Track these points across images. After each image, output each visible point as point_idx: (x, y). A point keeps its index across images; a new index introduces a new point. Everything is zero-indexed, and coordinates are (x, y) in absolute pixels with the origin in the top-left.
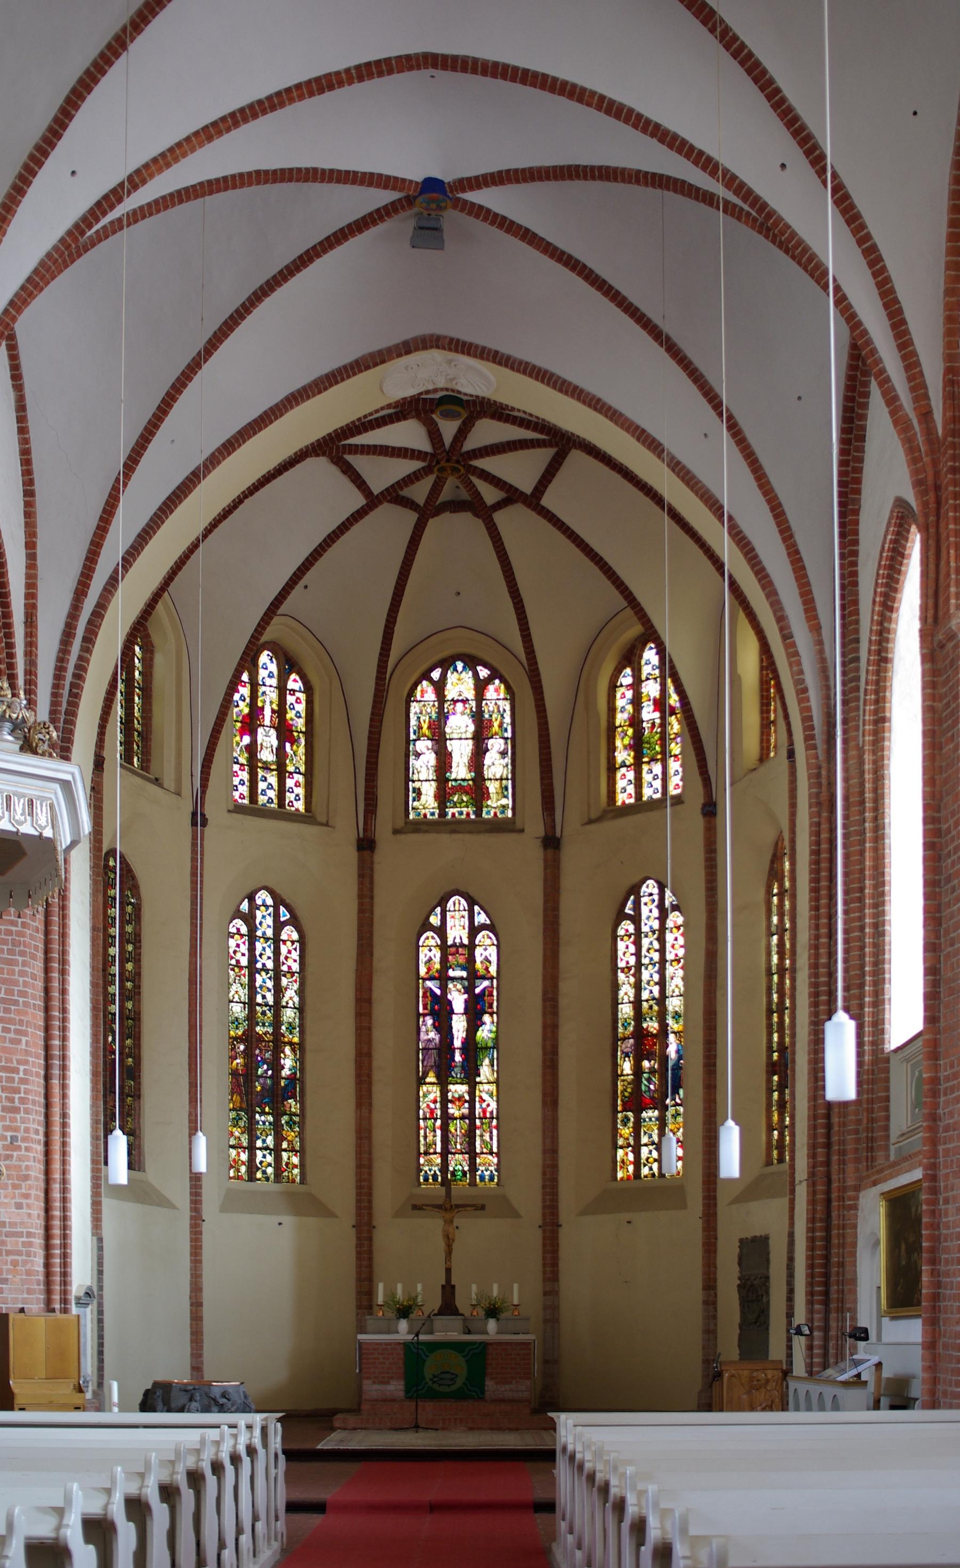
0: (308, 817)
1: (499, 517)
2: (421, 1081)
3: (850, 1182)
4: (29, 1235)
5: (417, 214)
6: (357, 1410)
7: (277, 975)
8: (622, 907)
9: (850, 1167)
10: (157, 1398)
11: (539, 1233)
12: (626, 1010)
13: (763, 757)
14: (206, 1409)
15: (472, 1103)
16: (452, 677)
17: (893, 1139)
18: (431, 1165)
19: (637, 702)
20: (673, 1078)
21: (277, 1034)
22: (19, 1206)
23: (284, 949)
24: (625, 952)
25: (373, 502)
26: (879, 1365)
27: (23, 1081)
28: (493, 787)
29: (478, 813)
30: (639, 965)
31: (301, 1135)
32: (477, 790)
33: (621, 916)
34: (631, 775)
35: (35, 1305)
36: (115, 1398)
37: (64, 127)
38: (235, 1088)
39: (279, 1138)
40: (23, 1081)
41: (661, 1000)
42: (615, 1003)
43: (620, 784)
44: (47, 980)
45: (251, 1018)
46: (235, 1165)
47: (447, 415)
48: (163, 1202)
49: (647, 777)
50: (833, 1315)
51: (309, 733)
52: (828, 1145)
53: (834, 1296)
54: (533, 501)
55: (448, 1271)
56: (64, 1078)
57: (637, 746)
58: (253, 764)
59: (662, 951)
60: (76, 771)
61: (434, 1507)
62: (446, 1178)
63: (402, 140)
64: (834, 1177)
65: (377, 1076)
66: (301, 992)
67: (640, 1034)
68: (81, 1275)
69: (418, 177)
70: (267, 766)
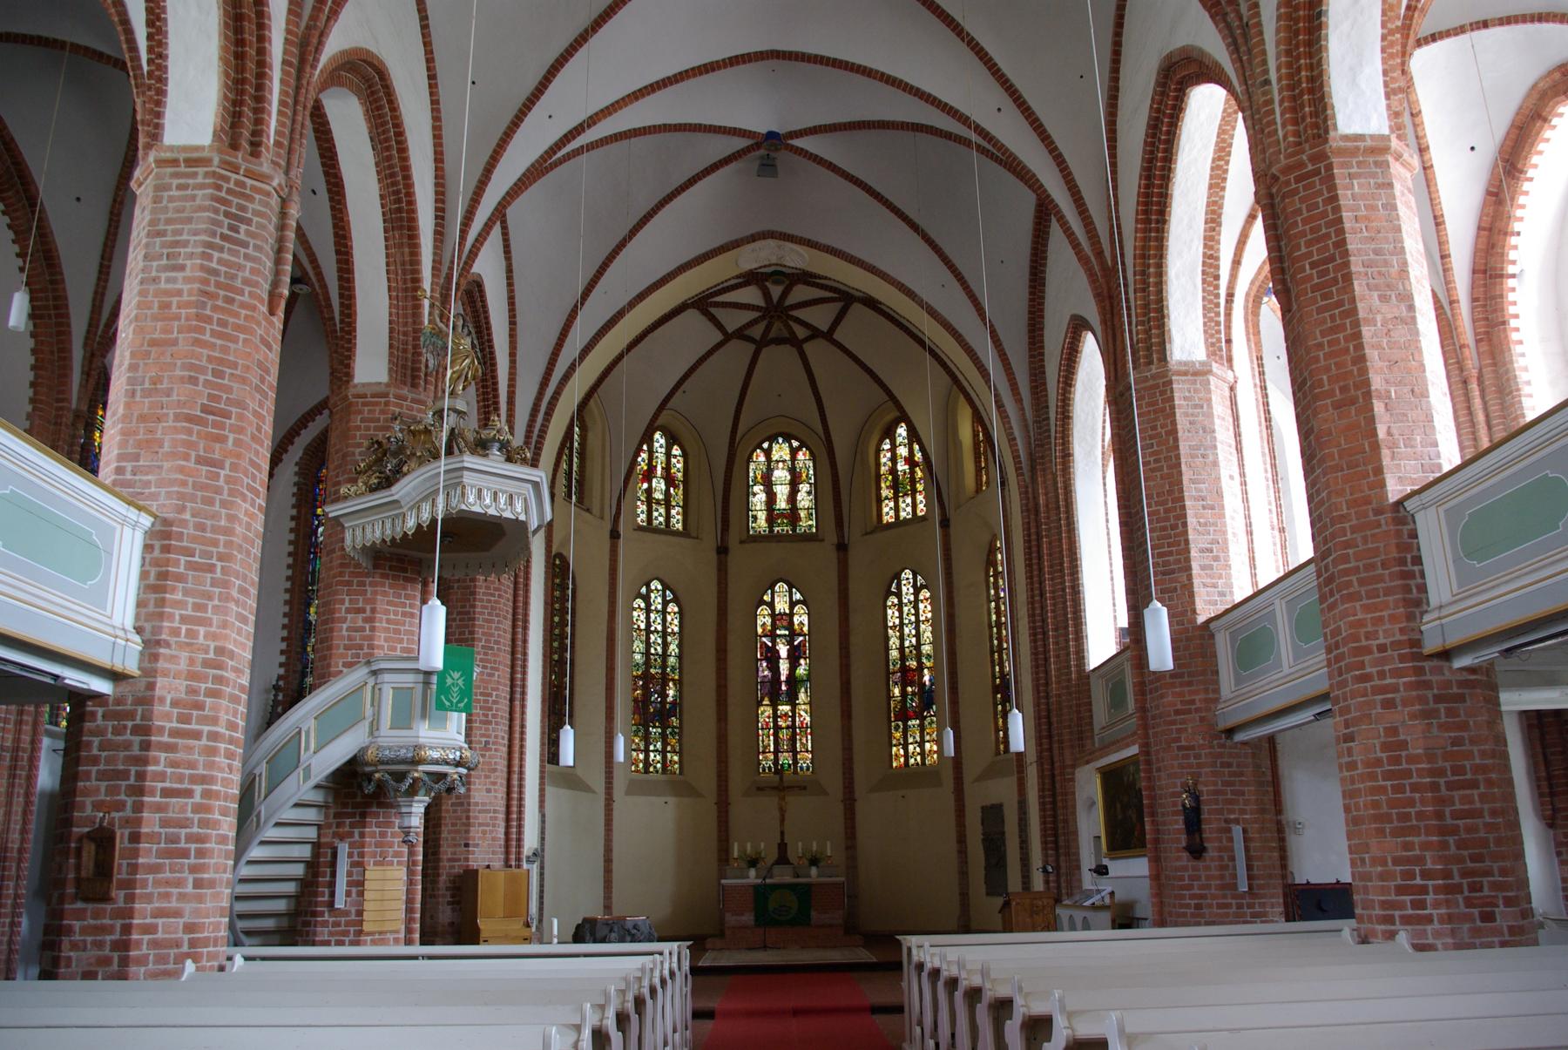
0: (685, 533)
1: (807, 347)
2: (760, 704)
3: (1069, 762)
4: (495, 811)
5: (762, 157)
6: (721, 934)
7: (664, 634)
8: (889, 588)
9: (1067, 753)
10: (585, 932)
11: (841, 807)
12: (894, 654)
13: (978, 490)
14: (622, 940)
15: (793, 717)
16: (775, 447)
17: (1096, 731)
18: (767, 761)
19: (894, 459)
20: (927, 698)
21: (664, 673)
22: (489, 791)
23: (669, 618)
24: (892, 616)
25: (728, 337)
26: (1112, 894)
27: (495, 702)
28: (803, 514)
29: (794, 530)
30: (902, 624)
31: (679, 741)
32: (793, 515)
33: (889, 593)
34: (892, 504)
35: (498, 863)
36: (555, 932)
37: (546, 87)
38: (636, 710)
39: (665, 744)
40: (495, 702)
41: (918, 646)
42: (887, 649)
43: (886, 510)
44: (514, 633)
45: (647, 663)
46: (635, 762)
47: (776, 283)
48: (587, 789)
49: (902, 505)
50: (1062, 858)
51: (686, 481)
52: (1050, 737)
53: (1061, 843)
54: (828, 336)
55: (782, 833)
56: (523, 700)
57: (895, 485)
58: (650, 500)
59: (917, 615)
60: (543, 475)
61: (796, 1012)
62: (779, 770)
63: (751, 108)
64: (1056, 759)
65: (730, 700)
66: (680, 646)
67: (904, 670)
68: (530, 841)
69: (764, 130)
70: (658, 500)
